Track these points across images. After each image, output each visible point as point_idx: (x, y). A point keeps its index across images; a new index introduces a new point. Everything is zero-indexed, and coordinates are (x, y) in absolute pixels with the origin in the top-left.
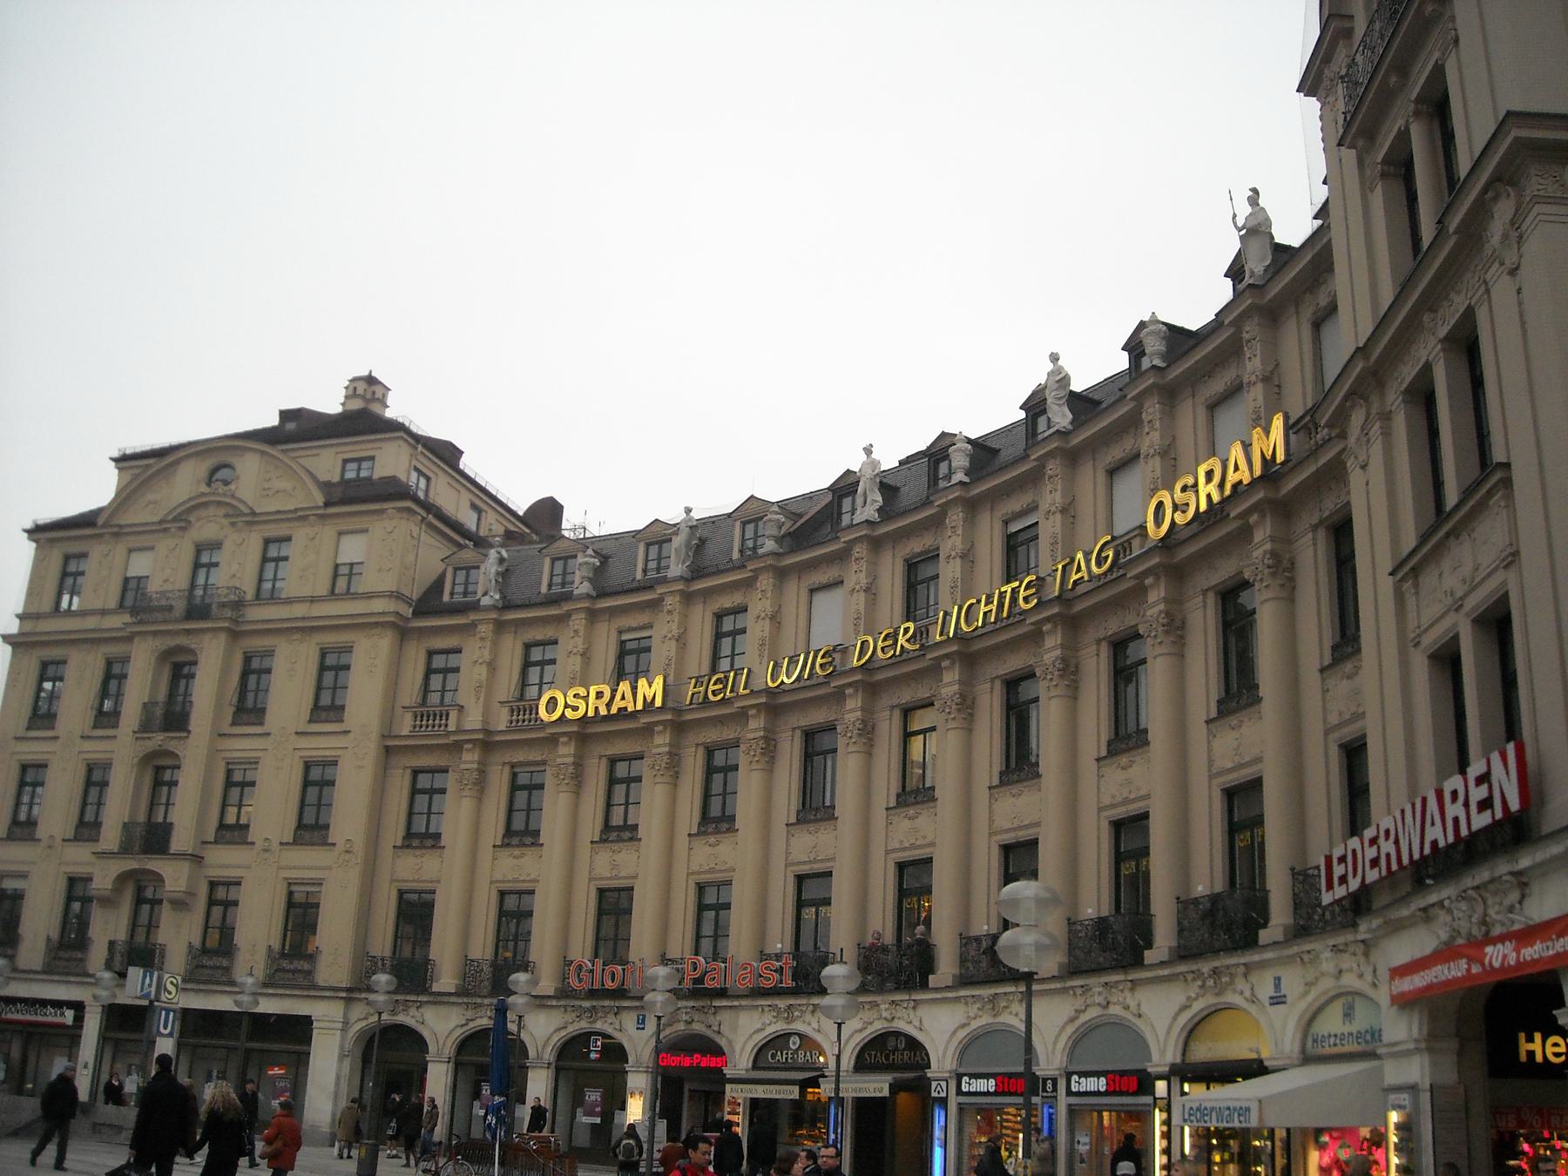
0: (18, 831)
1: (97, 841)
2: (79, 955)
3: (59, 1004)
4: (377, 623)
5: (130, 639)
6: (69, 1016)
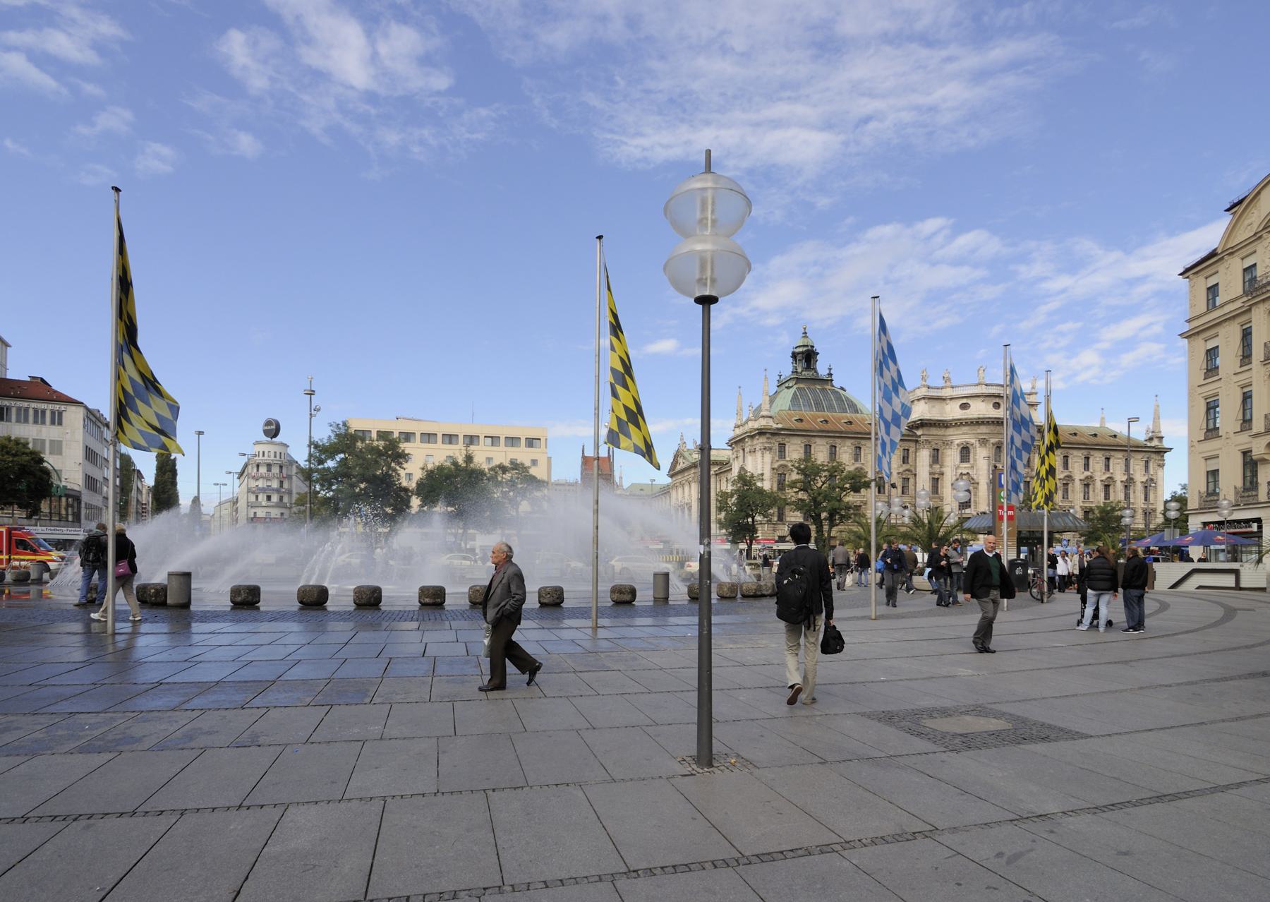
0: (1209, 434)
1: (1251, 429)
2: (1254, 493)
3: (1248, 522)
4: (1191, 335)
5: (1249, 310)
6: (1255, 527)
